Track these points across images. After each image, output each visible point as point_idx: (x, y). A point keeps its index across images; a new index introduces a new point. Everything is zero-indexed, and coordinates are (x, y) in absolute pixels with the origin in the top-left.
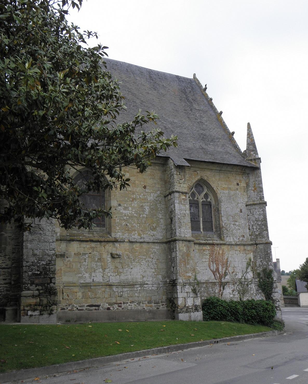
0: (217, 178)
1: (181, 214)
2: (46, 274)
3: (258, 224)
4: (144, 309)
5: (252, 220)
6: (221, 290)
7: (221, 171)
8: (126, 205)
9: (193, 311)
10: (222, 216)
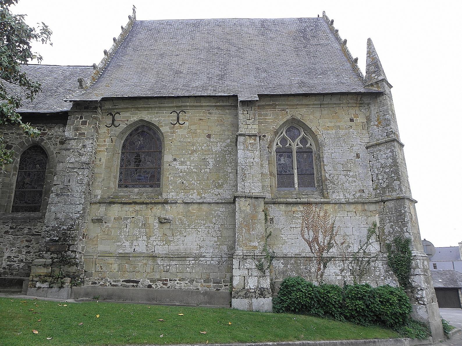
0: (318, 114)
1: (246, 163)
2: (65, 240)
3: (385, 172)
4: (198, 289)
5: (376, 167)
6: (320, 268)
7: (322, 106)
8: (182, 159)
9: (255, 297)
10: (324, 165)
